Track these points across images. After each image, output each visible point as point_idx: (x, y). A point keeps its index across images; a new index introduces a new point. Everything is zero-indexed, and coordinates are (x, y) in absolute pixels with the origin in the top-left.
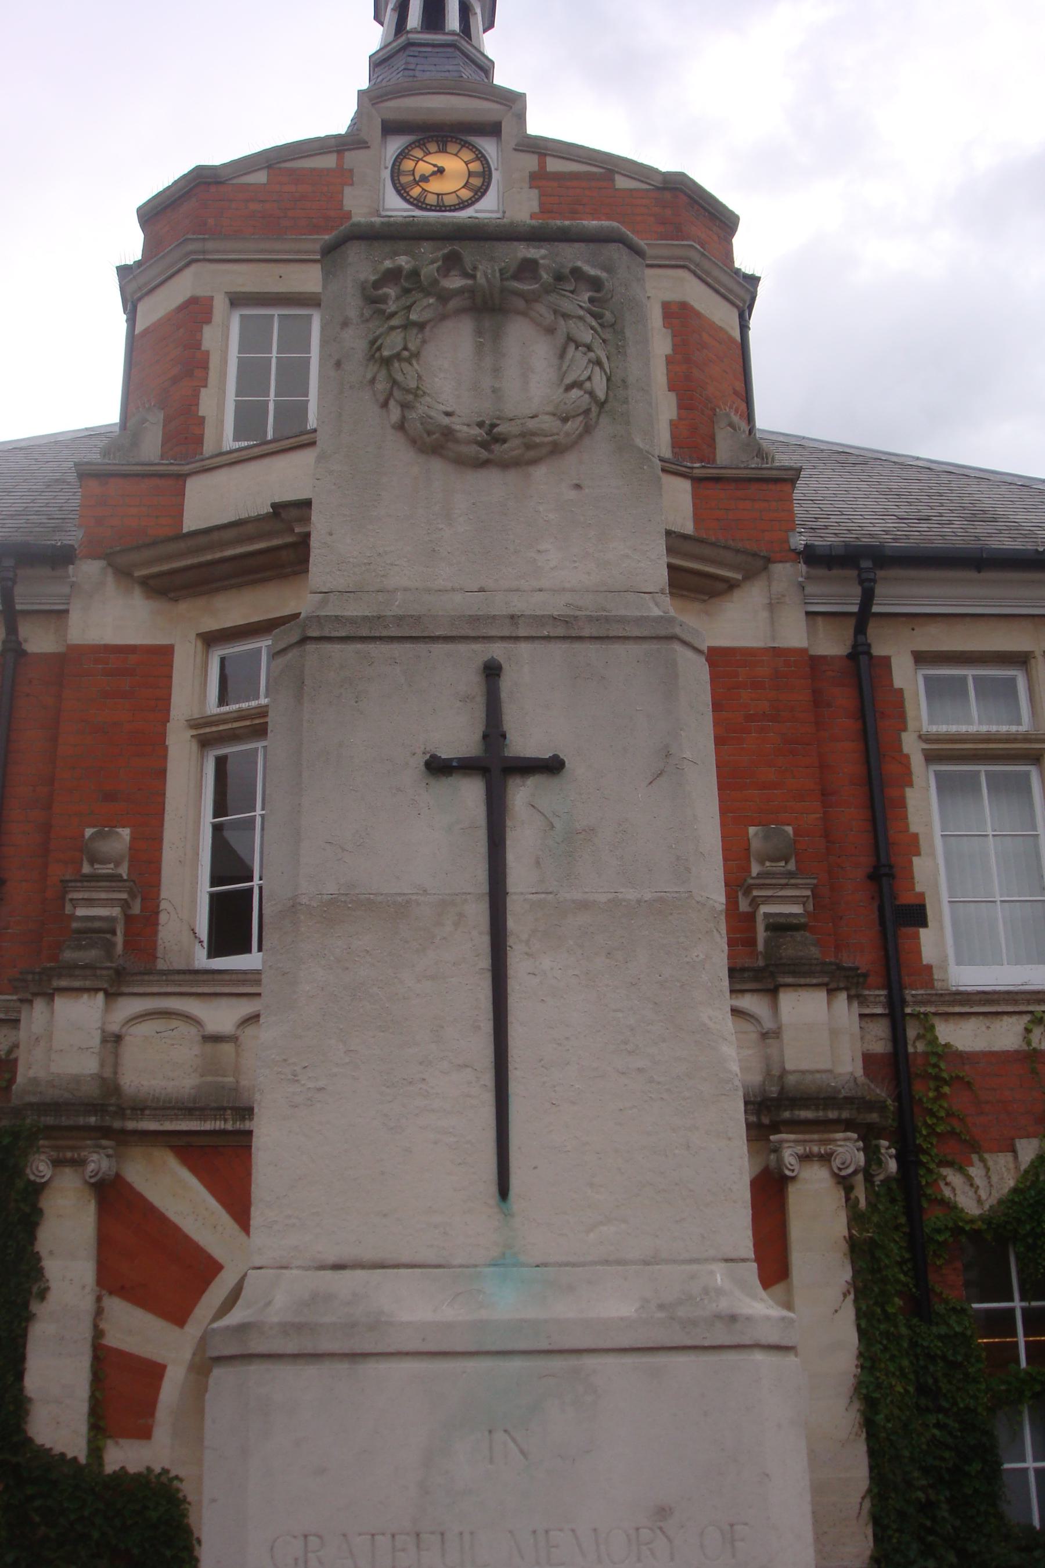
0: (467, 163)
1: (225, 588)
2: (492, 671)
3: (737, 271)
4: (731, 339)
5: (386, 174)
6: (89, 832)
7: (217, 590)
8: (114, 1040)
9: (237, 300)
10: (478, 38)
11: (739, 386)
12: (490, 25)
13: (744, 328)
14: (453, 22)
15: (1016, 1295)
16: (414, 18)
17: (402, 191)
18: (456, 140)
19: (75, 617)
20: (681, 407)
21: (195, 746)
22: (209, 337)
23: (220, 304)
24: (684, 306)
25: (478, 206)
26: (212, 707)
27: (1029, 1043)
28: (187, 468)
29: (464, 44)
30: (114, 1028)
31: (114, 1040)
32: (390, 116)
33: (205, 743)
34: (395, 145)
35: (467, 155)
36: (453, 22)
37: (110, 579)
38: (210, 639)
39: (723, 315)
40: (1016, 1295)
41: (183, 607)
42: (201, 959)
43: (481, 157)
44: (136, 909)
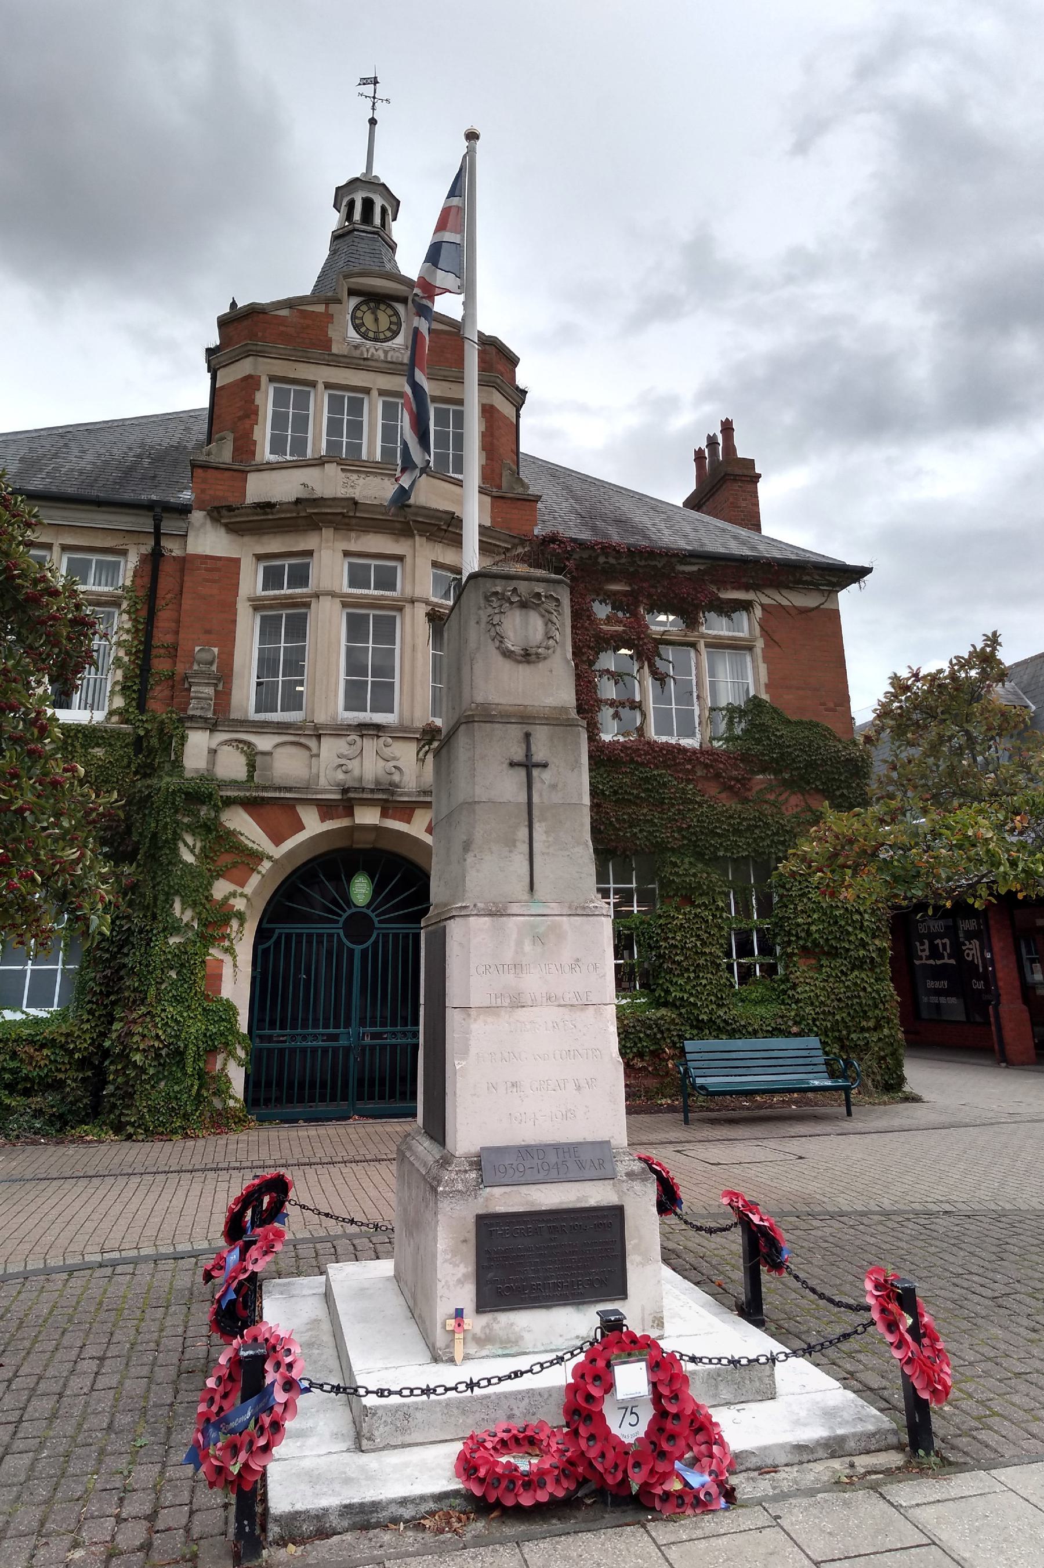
0: (391, 323)
1: (268, 533)
2: (528, 736)
3: (517, 388)
4: (512, 423)
5: (349, 317)
6: (197, 649)
7: (264, 533)
8: (213, 752)
9: (272, 379)
10: (389, 225)
11: (514, 447)
12: (394, 219)
13: (518, 416)
14: (377, 221)
15: (60, 963)
16: (357, 216)
17: (357, 328)
18: (385, 303)
19: (190, 539)
20: (487, 459)
21: (251, 610)
22: (259, 398)
23: (264, 380)
24: (492, 407)
25: (394, 341)
26: (259, 591)
27: (736, 1224)
28: (248, 469)
29: (382, 233)
30: (214, 746)
31: (213, 752)
32: (353, 286)
33: (256, 609)
34: (353, 302)
35: (390, 312)
36: (377, 221)
37: (208, 521)
38: (259, 558)
39: (508, 410)
40: (60, 963)
41: (246, 539)
42: (253, 716)
43: (396, 314)
44: (220, 688)
